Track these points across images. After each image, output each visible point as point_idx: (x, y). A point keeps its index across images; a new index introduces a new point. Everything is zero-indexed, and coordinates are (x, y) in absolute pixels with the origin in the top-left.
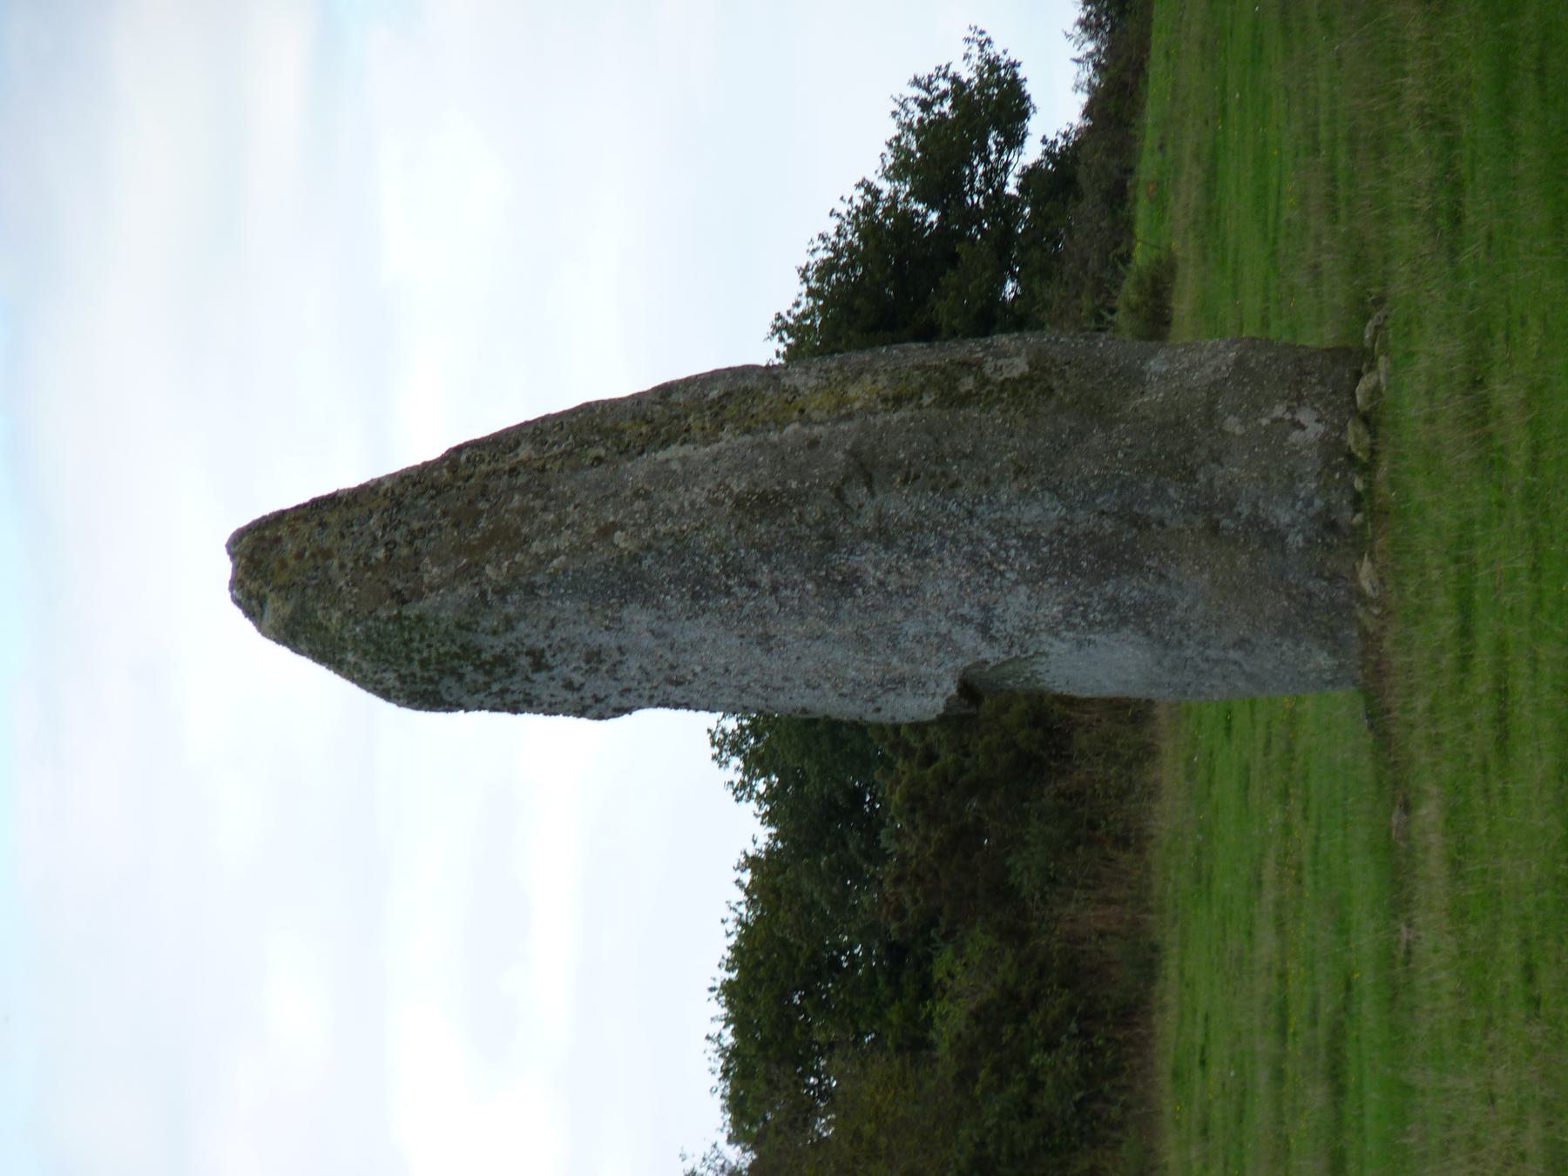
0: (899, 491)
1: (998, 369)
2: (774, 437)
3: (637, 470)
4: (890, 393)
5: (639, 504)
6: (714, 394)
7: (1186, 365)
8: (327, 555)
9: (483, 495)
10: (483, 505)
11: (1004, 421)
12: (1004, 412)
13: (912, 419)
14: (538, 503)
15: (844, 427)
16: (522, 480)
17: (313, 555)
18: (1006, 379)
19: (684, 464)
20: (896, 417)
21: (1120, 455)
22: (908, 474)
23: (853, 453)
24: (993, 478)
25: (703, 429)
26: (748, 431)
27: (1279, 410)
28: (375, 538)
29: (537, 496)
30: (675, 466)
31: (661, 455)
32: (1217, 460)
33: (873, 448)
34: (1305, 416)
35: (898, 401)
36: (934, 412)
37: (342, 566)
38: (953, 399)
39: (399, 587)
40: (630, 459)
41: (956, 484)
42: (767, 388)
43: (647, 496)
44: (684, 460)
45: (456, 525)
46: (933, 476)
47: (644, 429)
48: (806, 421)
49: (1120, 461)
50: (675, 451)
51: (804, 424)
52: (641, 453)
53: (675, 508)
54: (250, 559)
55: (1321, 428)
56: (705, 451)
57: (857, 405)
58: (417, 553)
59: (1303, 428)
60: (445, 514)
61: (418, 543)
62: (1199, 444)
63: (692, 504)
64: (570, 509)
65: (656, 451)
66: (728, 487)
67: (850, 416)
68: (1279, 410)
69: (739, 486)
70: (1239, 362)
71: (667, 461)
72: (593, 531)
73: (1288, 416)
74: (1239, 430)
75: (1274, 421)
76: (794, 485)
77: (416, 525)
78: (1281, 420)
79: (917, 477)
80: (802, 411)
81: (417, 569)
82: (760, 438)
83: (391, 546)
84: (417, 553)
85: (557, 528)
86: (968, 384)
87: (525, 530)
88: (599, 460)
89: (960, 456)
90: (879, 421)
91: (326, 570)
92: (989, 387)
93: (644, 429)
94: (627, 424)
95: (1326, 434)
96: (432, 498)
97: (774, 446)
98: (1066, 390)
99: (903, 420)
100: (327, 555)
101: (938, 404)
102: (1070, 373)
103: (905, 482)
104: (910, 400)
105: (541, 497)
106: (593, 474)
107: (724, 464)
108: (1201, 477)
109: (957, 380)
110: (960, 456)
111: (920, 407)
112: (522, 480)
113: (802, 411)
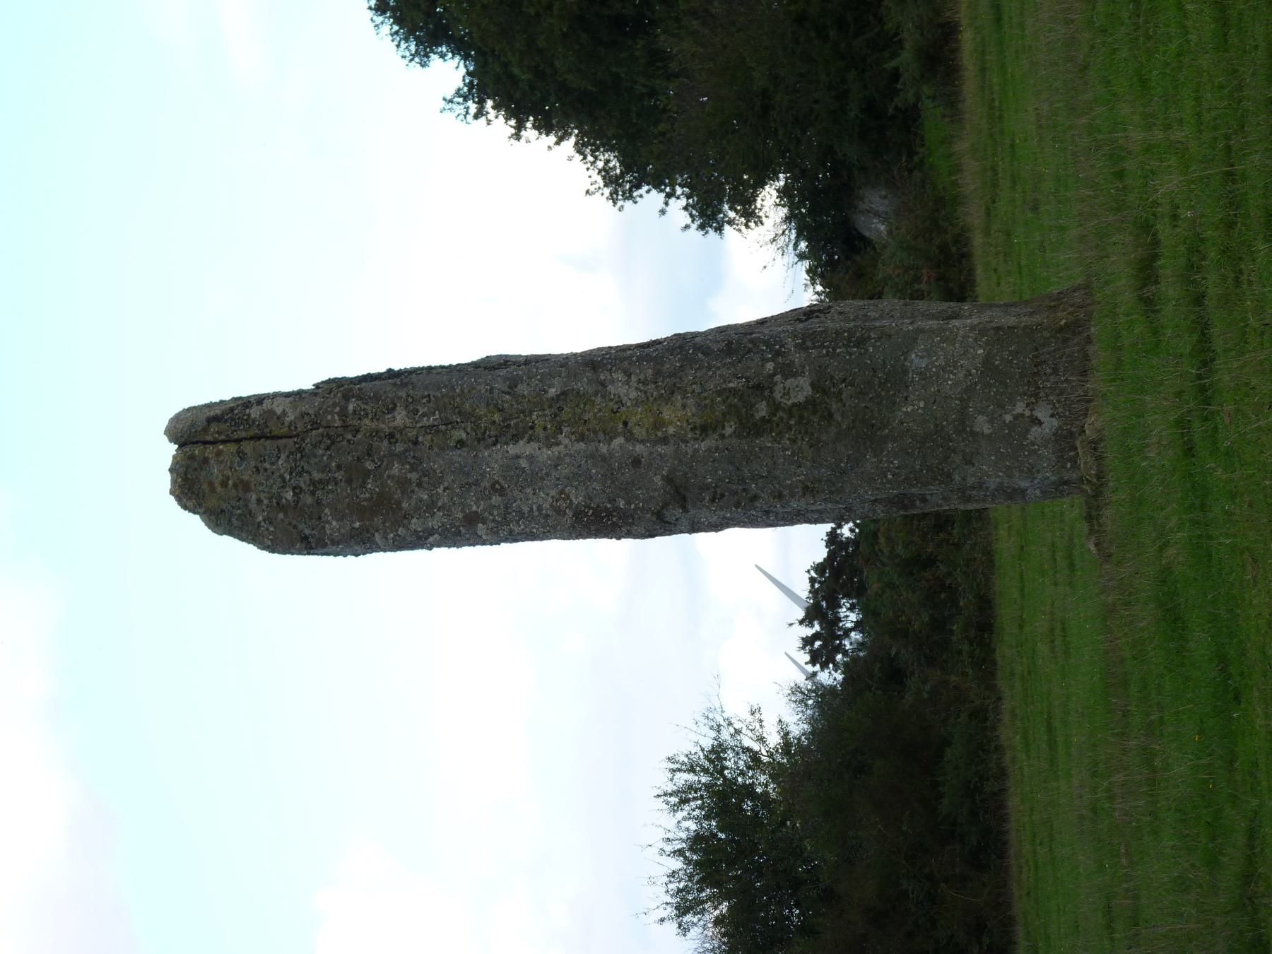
0: (708, 508)
1: (787, 394)
2: (604, 448)
3: (494, 459)
4: (698, 421)
5: (496, 499)
6: (552, 392)
7: (941, 362)
8: (246, 487)
9: (369, 455)
10: (369, 465)
11: (793, 454)
12: (794, 441)
13: (717, 449)
14: (414, 476)
15: (660, 449)
16: (399, 448)
17: (235, 486)
18: (794, 405)
19: (531, 463)
20: (703, 446)
21: (890, 476)
22: (715, 493)
23: (669, 480)
24: (786, 492)
25: (545, 429)
26: (582, 438)
27: (1020, 407)
28: (284, 480)
29: (413, 468)
30: (524, 464)
31: (512, 449)
32: (971, 463)
33: (685, 474)
34: (1042, 413)
35: (704, 430)
36: (734, 441)
37: (259, 501)
38: (752, 429)
39: (307, 532)
40: (487, 447)
41: (755, 498)
42: (596, 393)
43: (502, 492)
44: (531, 459)
45: (349, 481)
46: (736, 493)
47: (497, 417)
48: (630, 437)
49: (889, 482)
50: (522, 448)
51: (627, 440)
52: (494, 444)
53: (526, 509)
54: (185, 479)
55: (1055, 422)
56: (546, 454)
57: (671, 430)
58: (318, 503)
59: (1040, 423)
60: (339, 467)
61: (319, 493)
62: (954, 451)
63: (540, 508)
64: (440, 490)
65: (507, 444)
66: (568, 497)
67: (664, 440)
68: (1020, 407)
69: (578, 499)
70: (987, 361)
71: (518, 457)
72: (460, 516)
73: (1027, 413)
74: (987, 430)
75: (1016, 417)
76: (622, 504)
77: (317, 476)
78: (1022, 415)
79: (722, 496)
80: (625, 424)
81: (320, 518)
82: (592, 446)
83: (297, 490)
84: (318, 503)
85: (431, 507)
86: (762, 410)
87: (405, 505)
88: (461, 443)
89: (755, 478)
90: (688, 449)
91: (247, 502)
92: (780, 414)
93: (497, 417)
94: (481, 411)
95: (1060, 428)
96: (328, 448)
97: (604, 459)
98: (843, 415)
99: (709, 450)
100: (246, 487)
101: (737, 434)
102: (847, 391)
103: (713, 500)
104: (714, 430)
105: (415, 470)
106: (457, 456)
107: (564, 471)
108: (957, 478)
109: (752, 406)
110: (755, 478)
111: (723, 436)
112: (399, 448)
113: (625, 424)
